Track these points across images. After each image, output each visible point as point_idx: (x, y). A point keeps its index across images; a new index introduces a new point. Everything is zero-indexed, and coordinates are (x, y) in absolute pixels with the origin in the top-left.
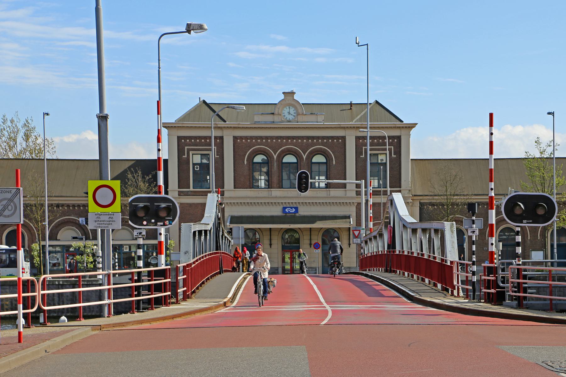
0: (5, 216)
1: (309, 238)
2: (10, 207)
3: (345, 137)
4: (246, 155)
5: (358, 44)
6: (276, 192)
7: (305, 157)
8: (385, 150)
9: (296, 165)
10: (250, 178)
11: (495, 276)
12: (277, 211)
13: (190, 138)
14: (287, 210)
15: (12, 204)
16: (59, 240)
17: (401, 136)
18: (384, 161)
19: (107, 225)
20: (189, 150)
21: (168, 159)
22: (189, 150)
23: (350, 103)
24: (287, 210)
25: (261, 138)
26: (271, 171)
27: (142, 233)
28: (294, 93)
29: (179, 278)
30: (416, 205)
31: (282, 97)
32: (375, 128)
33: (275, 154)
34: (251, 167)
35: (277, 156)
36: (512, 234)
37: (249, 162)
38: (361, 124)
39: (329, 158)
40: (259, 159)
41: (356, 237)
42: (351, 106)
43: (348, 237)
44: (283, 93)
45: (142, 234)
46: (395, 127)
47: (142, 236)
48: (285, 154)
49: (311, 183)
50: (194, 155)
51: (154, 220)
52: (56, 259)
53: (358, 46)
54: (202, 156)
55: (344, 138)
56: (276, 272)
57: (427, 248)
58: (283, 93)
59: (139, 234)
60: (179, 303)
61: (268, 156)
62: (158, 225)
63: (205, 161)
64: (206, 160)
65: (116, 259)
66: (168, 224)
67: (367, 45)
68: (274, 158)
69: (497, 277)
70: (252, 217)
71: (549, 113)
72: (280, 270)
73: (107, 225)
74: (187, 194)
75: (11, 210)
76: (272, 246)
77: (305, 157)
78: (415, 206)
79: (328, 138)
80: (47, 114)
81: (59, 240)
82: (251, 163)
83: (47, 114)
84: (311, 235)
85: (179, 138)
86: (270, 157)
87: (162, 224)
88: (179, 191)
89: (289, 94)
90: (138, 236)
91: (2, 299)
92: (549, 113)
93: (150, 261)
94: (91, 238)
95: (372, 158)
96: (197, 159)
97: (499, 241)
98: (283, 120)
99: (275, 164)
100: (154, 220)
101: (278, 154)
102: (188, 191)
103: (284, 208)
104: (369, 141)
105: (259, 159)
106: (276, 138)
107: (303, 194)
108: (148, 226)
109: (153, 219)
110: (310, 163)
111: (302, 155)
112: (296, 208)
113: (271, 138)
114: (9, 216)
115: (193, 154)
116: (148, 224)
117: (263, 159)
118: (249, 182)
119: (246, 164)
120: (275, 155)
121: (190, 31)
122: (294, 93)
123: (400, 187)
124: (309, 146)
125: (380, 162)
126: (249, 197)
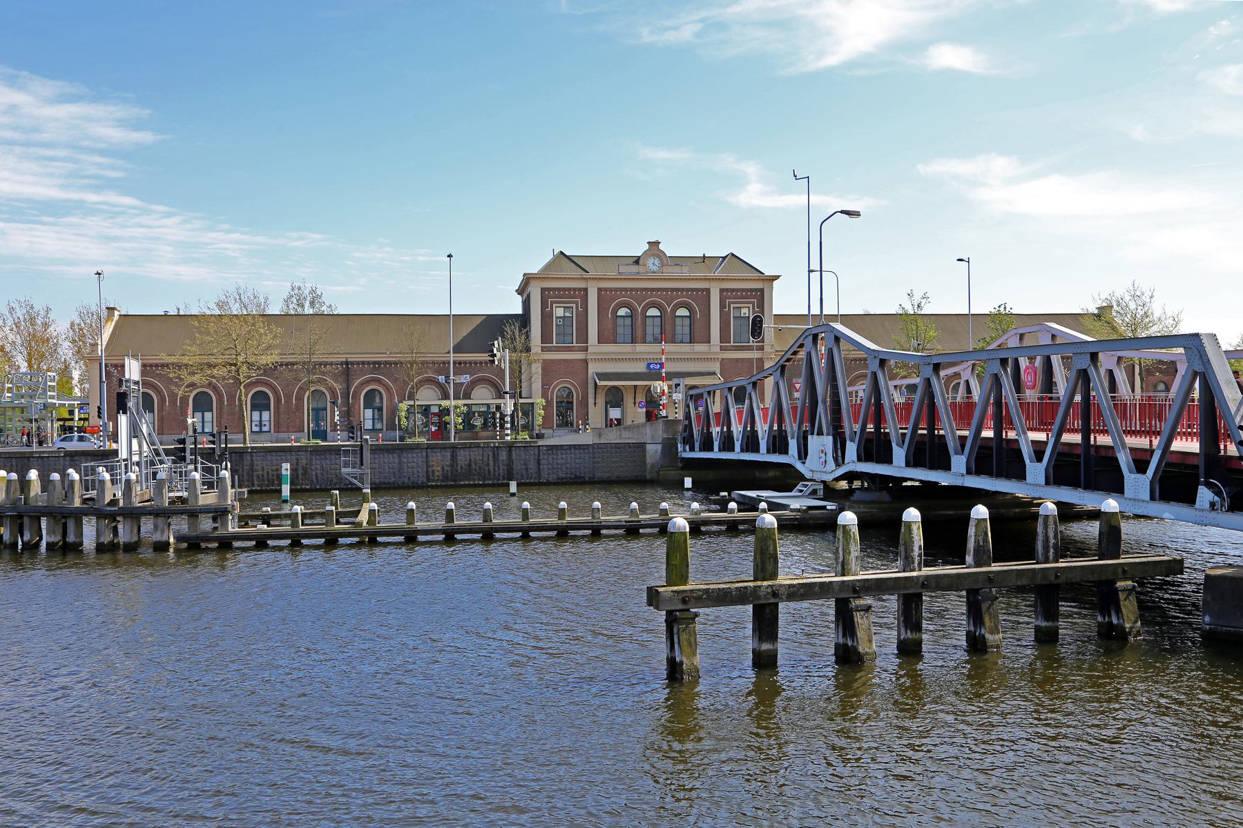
40: (622, 312)
55: (708, 290)
63: (568, 314)
70: (617, 374)
79: (692, 290)
96: (559, 312)
103: (649, 365)
105: (622, 312)
124: (673, 299)
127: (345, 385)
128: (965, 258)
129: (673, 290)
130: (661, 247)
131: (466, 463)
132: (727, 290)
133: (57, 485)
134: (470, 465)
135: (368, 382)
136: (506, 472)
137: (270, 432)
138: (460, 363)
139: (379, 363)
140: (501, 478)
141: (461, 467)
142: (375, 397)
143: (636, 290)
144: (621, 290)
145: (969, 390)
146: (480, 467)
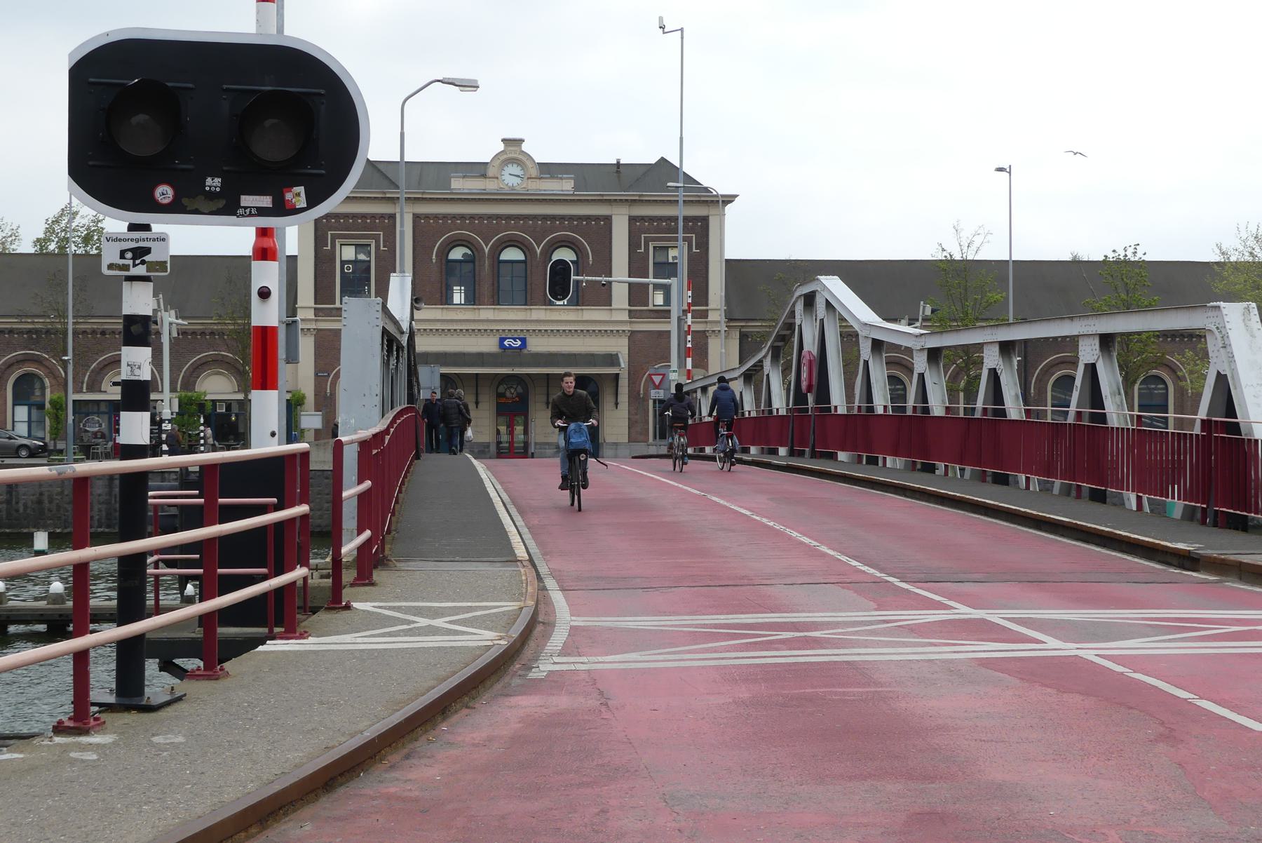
1: (546, 392)
3: (611, 216)
4: (435, 246)
5: (663, 29)
6: (487, 313)
7: (538, 251)
9: (524, 264)
10: (441, 288)
12: (488, 345)
14: (506, 343)
16: (105, 392)
17: (708, 216)
20: (334, 238)
21: (297, 256)
22: (334, 238)
23: (615, 162)
24: (506, 343)
26: (480, 275)
27: (147, 251)
28: (522, 141)
29: (345, 494)
30: (734, 337)
31: (501, 147)
33: (487, 246)
35: (490, 248)
37: (441, 260)
38: (640, 196)
39: (582, 252)
40: (457, 254)
41: (657, 387)
42: (618, 168)
43: (1086, 337)
44: (503, 140)
45: (147, 258)
46: (699, 202)
47: (152, 266)
48: (504, 245)
49: (577, 283)
50: (343, 247)
51: (218, 181)
52: (97, 425)
53: (664, 33)
54: (358, 248)
56: (487, 450)
57: (1235, 388)
58: (503, 140)
59: (129, 255)
60: (348, 607)
61: (474, 250)
62: (240, 211)
63: (362, 257)
64: (365, 254)
66: (301, 202)
67: (682, 30)
68: (485, 253)
71: (1000, 170)
72: (493, 449)
76: (480, 405)
77: (538, 251)
78: (732, 338)
79: (580, 218)
81: (105, 392)
82: (444, 262)
84: (548, 387)
86: (477, 249)
87: (266, 201)
88: (315, 309)
89: (513, 143)
90: (126, 268)
91: (12, 487)
92: (1000, 170)
95: (657, 254)
96: (349, 253)
97: (244, 433)
98: (502, 186)
99: (487, 262)
100: (218, 181)
101: (492, 245)
103: (502, 340)
104: (681, 224)
105: (457, 254)
106: (489, 218)
107: (277, 433)
109: (213, 176)
111: (534, 247)
112: (523, 340)
113: (481, 217)
115: (341, 245)
116: (185, 201)
117: (465, 255)
118: (440, 294)
119: (436, 262)
120: (487, 246)
122: (522, 141)
123: (707, 305)
125: (670, 260)
126: (438, 321)
128: (1006, 167)
129: (545, 218)
130: (524, 147)
131: (34, 498)
132: (642, 219)
133: (1083, 491)
134: (40, 502)
136: (104, 514)
138: (84, 332)
139: (37, 331)
140: (96, 523)
141: (25, 506)
142: (33, 388)
143: (534, 217)
144: (509, 217)
145: (1095, 395)
146: (58, 506)
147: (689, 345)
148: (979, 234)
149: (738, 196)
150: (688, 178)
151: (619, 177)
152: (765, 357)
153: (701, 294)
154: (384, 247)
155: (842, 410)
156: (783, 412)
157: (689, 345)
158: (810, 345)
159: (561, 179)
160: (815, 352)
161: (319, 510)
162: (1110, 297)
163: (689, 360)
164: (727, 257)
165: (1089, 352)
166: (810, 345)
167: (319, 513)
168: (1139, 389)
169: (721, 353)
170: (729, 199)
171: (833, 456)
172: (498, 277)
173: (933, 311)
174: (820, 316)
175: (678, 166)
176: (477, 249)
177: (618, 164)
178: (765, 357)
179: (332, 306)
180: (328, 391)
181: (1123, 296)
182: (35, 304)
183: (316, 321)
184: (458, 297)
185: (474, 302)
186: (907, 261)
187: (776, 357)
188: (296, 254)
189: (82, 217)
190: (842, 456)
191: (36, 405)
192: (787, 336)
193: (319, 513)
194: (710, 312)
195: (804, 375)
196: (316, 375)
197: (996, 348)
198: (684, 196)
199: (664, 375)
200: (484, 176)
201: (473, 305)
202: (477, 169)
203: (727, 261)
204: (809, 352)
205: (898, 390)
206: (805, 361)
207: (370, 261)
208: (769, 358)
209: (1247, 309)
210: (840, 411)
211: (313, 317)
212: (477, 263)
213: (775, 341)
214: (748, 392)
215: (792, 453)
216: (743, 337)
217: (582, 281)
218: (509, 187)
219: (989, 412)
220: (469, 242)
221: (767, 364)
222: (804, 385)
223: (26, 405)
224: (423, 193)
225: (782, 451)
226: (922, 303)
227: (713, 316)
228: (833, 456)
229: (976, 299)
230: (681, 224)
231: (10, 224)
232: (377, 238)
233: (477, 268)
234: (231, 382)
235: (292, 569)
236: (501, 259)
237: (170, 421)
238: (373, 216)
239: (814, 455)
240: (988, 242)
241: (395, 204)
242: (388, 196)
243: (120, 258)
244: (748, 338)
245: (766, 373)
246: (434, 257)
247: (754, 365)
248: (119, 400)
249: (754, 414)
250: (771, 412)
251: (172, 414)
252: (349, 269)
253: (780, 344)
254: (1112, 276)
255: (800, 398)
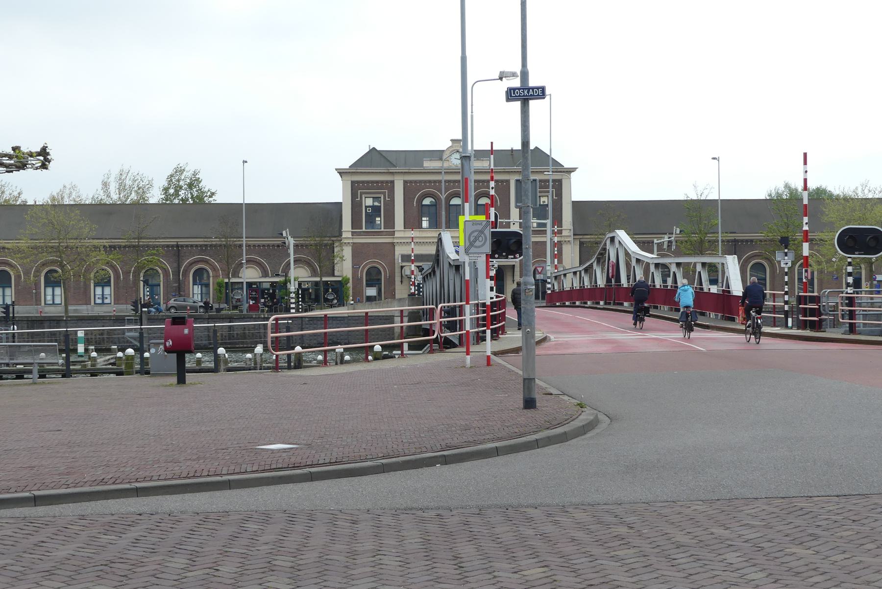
0: (476, 247)
2: (480, 239)
8: (548, 192)
11: (817, 305)
13: (363, 182)
15: (482, 235)
16: (241, 277)
18: (546, 203)
19: (476, 258)
20: (361, 194)
21: (341, 203)
22: (361, 194)
25: (430, 182)
31: (450, 144)
32: (556, 172)
34: (420, 209)
36: (666, 270)
40: (427, 201)
41: (540, 273)
42: (512, 152)
44: (451, 140)
48: (452, 197)
58: (451, 140)
63: (376, 204)
64: (378, 202)
65: (300, 294)
69: (819, 306)
71: (714, 158)
73: (476, 258)
74: (359, 234)
75: (482, 240)
80: (246, 162)
81: (241, 277)
82: (420, 205)
83: (246, 162)
85: (353, 183)
86: (438, 199)
87: (513, 257)
88: (352, 232)
92: (714, 158)
93: (327, 296)
94: (270, 276)
96: (369, 202)
102: (361, 232)
104: (551, 184)
105: (427, 201)
108: (500, 259)
110: (448, 206)
114: (479, 247)
115: (365, 197)
117: (431, 202)
121: (502, 78)
123: (562, 227)
127: (175, 265)
135: (44, 265)
137: (61, 304)
147: (556, 253)
148: (706, 189)
149: (577, 168)
150: (555, 163)
151: (513, 157)
152: (594, 262)
153: (558, 220)
154: (388, 198)
155: (625, 285)
156: (602, 286)
157: (556, 253)
158: (613, 259)
159: (483, 160)
160: (615, 261)
161: (376, 335)
162: (778, 221)
163: (556, 260)
164: (573, 200)
165: (699, 268)
166: (613, 259)
167: (377, 337)
168: (798, 270)
169: (572, 256)
170: (573, 170)
171: (622, 304)
172: (449, 213)
173: (680, 232)
174: (617, 247)
175: (549, 155)
176: (438, 199)
177: (512, 150)
178: (594, 262)
179: (361, 230)
180: (359, 276)
181: (785, 220)
182: (212, 232)
183: (353, 238)
184: (425, 224)
185: (437, 226)
186: (671, 200)
187: (598, 262)
188: (342, 201)
189: (187, 172)
190: (626, 304)
191: (205, 285)
192: (602, 258)
193: (377, 337)
194: (563, 231)
195: (610, 271)
196: (353, 267)
197: (675, 265)
198: (552, 169)
199: (543, 267)
200: (441, 159)
201: (436, 228)
202: (437, 155)
203: (573, 201)
204: (613, 261)
205: (666, 271)
206: (610, 265)
207: (380, 206)
208: (596, 262)
209: (734, 257)
210: (624, 286)
211: (351, 236)
212: (438, 206)
213: (598, 255)
214: (586, 277)
215: (606, 304)
216: (581, 244)
217: (503, 222)
218: (455, 165)
219: (673, 287)
220: (433, 195)
221: (595, 265)
222: (610, 275)
223: (100, 286)
224: (409, 169)
225: (602, 303)
226: (675, 227)
227: (564, 233)
228: (622, 304)
229: (705, 224)
230: (551, 184)
231: (147, 177)
232: (384, 193)
233: (438, 208)
234: (257, 270)
235: (502, 322)
236: (451, 203)
237: (294, 293)
238: (382, 182)
239: (615, 304)
240: (712, 192)
241: (394, 175)
242: (390, 171)
243: (12, 148)
244: (584, 244)
245: (594, 269)
246: (415, 203)
247: (589, 265)
248: (741, 296)
249: (589, 287)
250: (596, 286)
251: (295, 289)
252: (370, 210)
253: (600, 256)
254: (779, 210)
255: (609, 280)
